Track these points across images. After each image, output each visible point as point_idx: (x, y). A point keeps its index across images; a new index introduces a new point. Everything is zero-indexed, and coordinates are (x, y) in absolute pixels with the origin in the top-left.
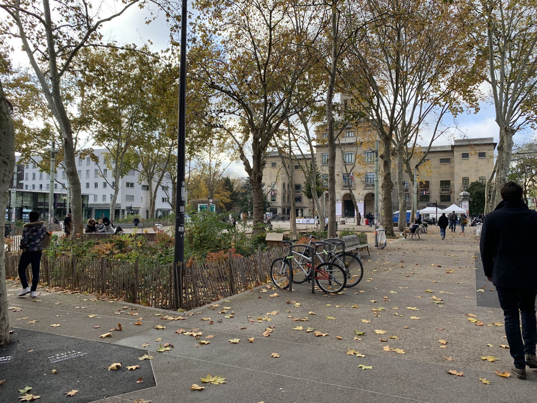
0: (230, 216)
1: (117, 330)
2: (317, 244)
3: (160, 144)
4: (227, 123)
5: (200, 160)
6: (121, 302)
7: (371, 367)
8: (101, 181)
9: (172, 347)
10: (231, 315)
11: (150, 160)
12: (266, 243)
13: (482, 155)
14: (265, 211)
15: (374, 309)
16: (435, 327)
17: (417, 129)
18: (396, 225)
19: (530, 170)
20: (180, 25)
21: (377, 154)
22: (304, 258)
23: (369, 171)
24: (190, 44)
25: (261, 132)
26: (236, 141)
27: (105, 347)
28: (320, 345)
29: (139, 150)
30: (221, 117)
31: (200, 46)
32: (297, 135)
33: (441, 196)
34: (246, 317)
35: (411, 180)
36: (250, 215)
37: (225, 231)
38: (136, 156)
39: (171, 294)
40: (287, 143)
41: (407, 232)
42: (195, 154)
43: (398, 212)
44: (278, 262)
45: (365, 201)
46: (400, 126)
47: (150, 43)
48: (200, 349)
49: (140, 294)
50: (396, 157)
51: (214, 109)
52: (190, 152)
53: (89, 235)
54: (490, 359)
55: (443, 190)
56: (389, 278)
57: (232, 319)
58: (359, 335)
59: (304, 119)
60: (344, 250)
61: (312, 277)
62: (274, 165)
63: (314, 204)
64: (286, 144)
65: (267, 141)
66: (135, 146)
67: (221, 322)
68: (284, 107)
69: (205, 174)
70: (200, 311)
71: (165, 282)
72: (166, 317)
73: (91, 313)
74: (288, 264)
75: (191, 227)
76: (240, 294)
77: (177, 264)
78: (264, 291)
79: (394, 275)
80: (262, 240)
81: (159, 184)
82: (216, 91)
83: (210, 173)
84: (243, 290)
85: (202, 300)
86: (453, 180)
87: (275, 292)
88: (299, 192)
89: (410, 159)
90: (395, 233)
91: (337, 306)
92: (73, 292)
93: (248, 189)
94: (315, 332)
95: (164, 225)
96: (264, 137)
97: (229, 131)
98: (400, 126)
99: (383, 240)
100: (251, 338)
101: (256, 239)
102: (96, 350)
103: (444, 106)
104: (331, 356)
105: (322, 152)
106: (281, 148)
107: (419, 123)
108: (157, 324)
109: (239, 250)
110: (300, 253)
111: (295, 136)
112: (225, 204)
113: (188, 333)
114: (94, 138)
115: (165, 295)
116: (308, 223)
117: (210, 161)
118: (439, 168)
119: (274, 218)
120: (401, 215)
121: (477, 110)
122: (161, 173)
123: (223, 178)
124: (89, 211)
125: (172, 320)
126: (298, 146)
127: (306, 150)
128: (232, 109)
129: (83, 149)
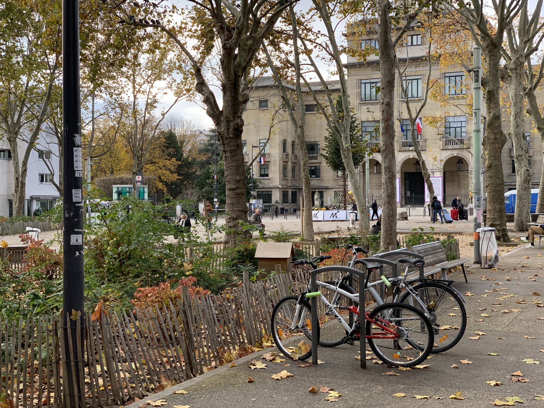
0: (178, 208)
2: (370, 265)
4: (168, 17)
5: (114, 96)
11: (12, 96)
12: (256, 262)
14: (249, 196)
18: (511, 219)
21: (477, 76)
22: (341, 295)
23: (452, 114)
25: (239, 34)
26: (188, 53)
32: (310, 40)
36: (217, 206)
37: (170, 239)
39: (58, 377)
40: (292, 58)
41: (534, 233)
42: (102, 83)
43: (514, 192)
44: (286, 304)
45: (444, 173)
46: (516, 22)
50: (510, 84)
52: (92, 80)
56: (516, 328)
59: (325, 9)
60: (422, 273)
62: (263, 104)
63: (345, 181)
64: (288, 61)
65: (251, 51)
69: (124, 125)
71: (44, 355)
74: (309, 307)
75: (99, 234)
77: (71, 314)
78: (260, 365)
79: (524, 323)
81: (31, 145)
83: (136, 122)
84: (213, 364)
85: (126, 390)
87: (281, 367)
88: (316, 158)
89: (535, 87)
90: (510, 234)
93: (213, 153)
96: (246, 45)
97: (172, 34)
98: (516, 22)
99: (492, 250)
101: (236, 255)
105: (359, 77)
106: (278, 68)
110: (333, 283)
111: (307, 43)
112: (166, 184)
116: (335, 218)
117: (135, 97)
119: (265, 211)
120: (520, 198)
122: (35, 123)
123: (162, 133)
126: (313, 64)
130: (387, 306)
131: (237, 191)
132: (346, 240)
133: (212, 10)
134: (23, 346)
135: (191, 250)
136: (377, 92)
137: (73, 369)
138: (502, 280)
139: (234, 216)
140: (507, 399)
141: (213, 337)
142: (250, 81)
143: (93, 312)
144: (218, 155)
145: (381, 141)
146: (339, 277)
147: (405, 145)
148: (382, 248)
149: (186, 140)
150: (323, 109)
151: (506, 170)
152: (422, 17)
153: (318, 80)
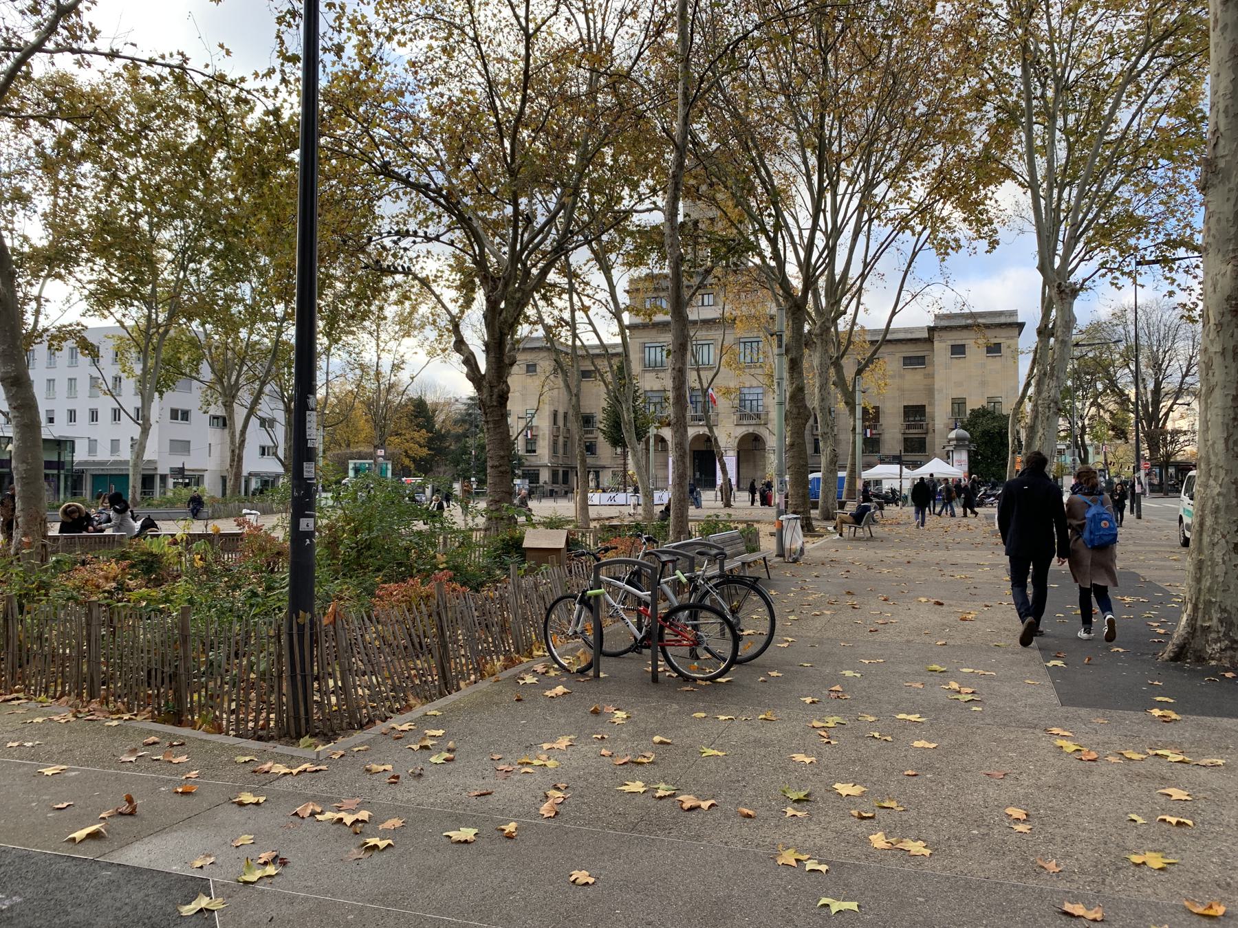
1: (121, 814)
2: (664, 558)
3: (254, 314)
6: (142, 722)
7: (853, 905)
8: (105, 405)
9: (284, 863)
10: (447, 755)
11: (230, 354)
12: (524, 553)
13: (994, 349)
15: (816, 724)
16: (980, 768)
17: (860, 289)
18: (815, 506)
19: (1092, 383)
20: (302, 12)
21: (780, 340)
23: (747, 385)
24: (327, 58)
25: (506, 285)
26: (444, 306)
27: (81, 872)
28: (698, 837)
29: (201, 329)
30: (405, 249)
31: (355, 72)
32: (588, 296)
33: (906, 440)
34: (489, 757)
35: (847, 403)
37: (419, 525)
38: (194, 343)
39: (280, 694)
40: (567, 315)
41: (843, 522)
43: (818, 475)
46: (822, 282)
47: (224, 52)
48: (365, 865)
49: (196, 697)
51: (387, 228)
52: (328, 335)
53: (66, 538)
54: (1155, 861)
55: (908, 427)
56: (830, 634)
57: (451, 766)
58: (798, 801)
61: (652, 640)
62: (531, 368)
64: (562, 319)
66: (190, 320)
67: (420, 775)
68: (557, 230)
70: (362, 744)
71: (263, 666)
72: (266, 767)
73: (51, 759)
74: (591, 608)
76: (465, 693)
77: (298, 617)
78: (530, 679)
79: (839, 627)
80: (514, 546)
81: (251, 411)
82: (394, 185)
84: (473, 678)
85: (365, 711)
86: (932, 404)
88: (591, 432)
89: (842, 356)
90: (814, 523)
91: (722, 718)
92: (8, 697)
93: (471, 424)
94: (681, 798)
95: (264, 512)
97: (425, 282)
98: (822, 282)
100: (507, 822)
101: (500, 545)
102: (51, 886)
103: (920, 234)
104: (735, 873)
105: (642, 340)
106: (550, 327)
107: (863, 276)
108: (241, 789)
109: (458, 573)
110: (618, 579)
111: (584, 298)
112: (414, 460)
113: (329, 815)
114: (87, 298)
115: (265, 698)
118: (902, 377)
119: (531, 494)
120: (825, 482)
121: (993, 244)
122: (257, 385)
123: (410, 399)
124: (75, 480)
125: (285, 774)
126: (591, 323)
127: (610, 335)
128: (432, 230)
129: (57, 324)
130: (681, 608)
131: (501, 469)
132: (629, 528)
133: (474, 257)
134: (237, 655)
135: (445, 539)
136: (668, 355)
137: (299, 685)
138: (809, 576)
139: (497, 498)
140: (827, 719)
141: (471, 641)
142: (518, 341)
143: (324, 614)
144: (477, 426)
145: (670, 411)
146: (625, 572)
147: (694, 418)
148: (671, 538)
149: (440, 408)
150: (602, 376)
151: (810, 449)
152: (718, 271)
153: (597, 342)
